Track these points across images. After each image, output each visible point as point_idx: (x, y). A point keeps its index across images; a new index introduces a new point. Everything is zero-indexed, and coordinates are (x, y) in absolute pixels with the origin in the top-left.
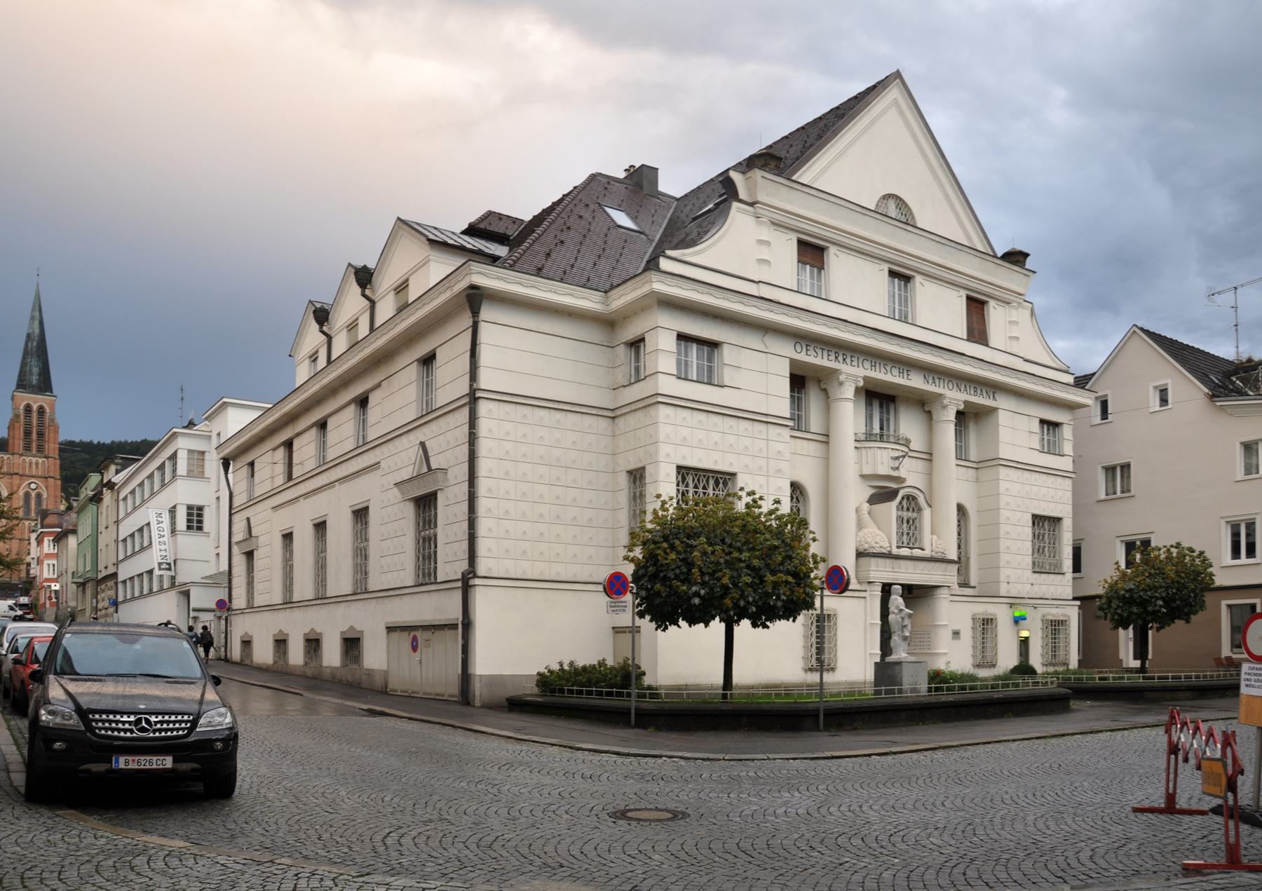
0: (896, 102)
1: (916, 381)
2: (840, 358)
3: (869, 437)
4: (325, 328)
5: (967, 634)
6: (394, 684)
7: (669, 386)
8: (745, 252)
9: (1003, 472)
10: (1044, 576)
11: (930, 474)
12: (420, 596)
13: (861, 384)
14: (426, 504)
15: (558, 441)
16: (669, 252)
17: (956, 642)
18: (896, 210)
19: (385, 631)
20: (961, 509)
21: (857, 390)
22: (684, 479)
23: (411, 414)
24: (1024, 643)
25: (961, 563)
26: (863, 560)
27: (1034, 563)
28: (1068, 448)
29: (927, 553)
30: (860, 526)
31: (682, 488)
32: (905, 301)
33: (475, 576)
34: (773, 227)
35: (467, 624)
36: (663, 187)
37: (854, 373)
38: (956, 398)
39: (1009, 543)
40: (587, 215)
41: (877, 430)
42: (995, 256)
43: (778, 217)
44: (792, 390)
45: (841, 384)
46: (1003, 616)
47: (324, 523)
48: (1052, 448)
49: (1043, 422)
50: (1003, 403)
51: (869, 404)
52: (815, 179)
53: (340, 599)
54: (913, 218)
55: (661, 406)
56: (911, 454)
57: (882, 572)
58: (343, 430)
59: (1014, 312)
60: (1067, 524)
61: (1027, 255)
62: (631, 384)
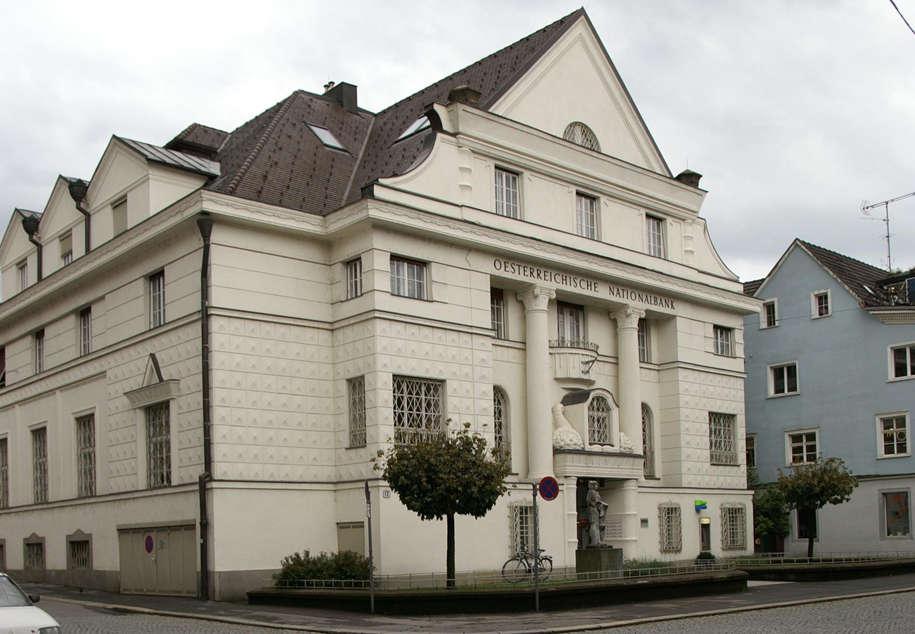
0: (581, 37)
1: (603, 293)
2: (535, 274)
3: (561, 344)
4: (35, 238)
5: (654, 522)
6: (127, 584)
7: (384, 302)
8: (447, 179)
9: (682, 374)
10: (721, 468)
11: (617, 376)
12: (155, 499)
13: (554, 296)
14: (157, 413)
15: (283, 352)
16: (381, 181)
17: (644, 529)
18: (582, 137)
19: (116, 534)
20: (645, 408)
21: (550, 301)
22: (399, 387)
23: (141, 325)
24: (705, 528)
25: (647, 457)
26: (560, 457)
27: (712, 456)
28: (740, 351)
29: (616, 449)
30: (556, 425)
31: (398, 395)
32: (593, 220)
33: (212, 480)
34: (473, 155)
35: (205, 525)
36: (363, 102)
37: (547, 287)
38: (638, 307)
39: (688, 438)
40: (295, 134)
41: (568, 337)
42: (671, 178)
43: (478, 146)
44: (492, 303)
45: (536, 297)
46: (686, 505)
47: (44, 429)
48: (724, 351)
49: (716, 327)
50: (680, 310)
51: (560, 312)
52: (511, 109)
53: (64, 504)
54: (597, 143)
55: (378, 321)
56: (599, 358)
57: (578, 467)
58: (63, 340)
59: (689, 228)
60: (741, 420)
61: (700, 176)
62: (347, 300)
